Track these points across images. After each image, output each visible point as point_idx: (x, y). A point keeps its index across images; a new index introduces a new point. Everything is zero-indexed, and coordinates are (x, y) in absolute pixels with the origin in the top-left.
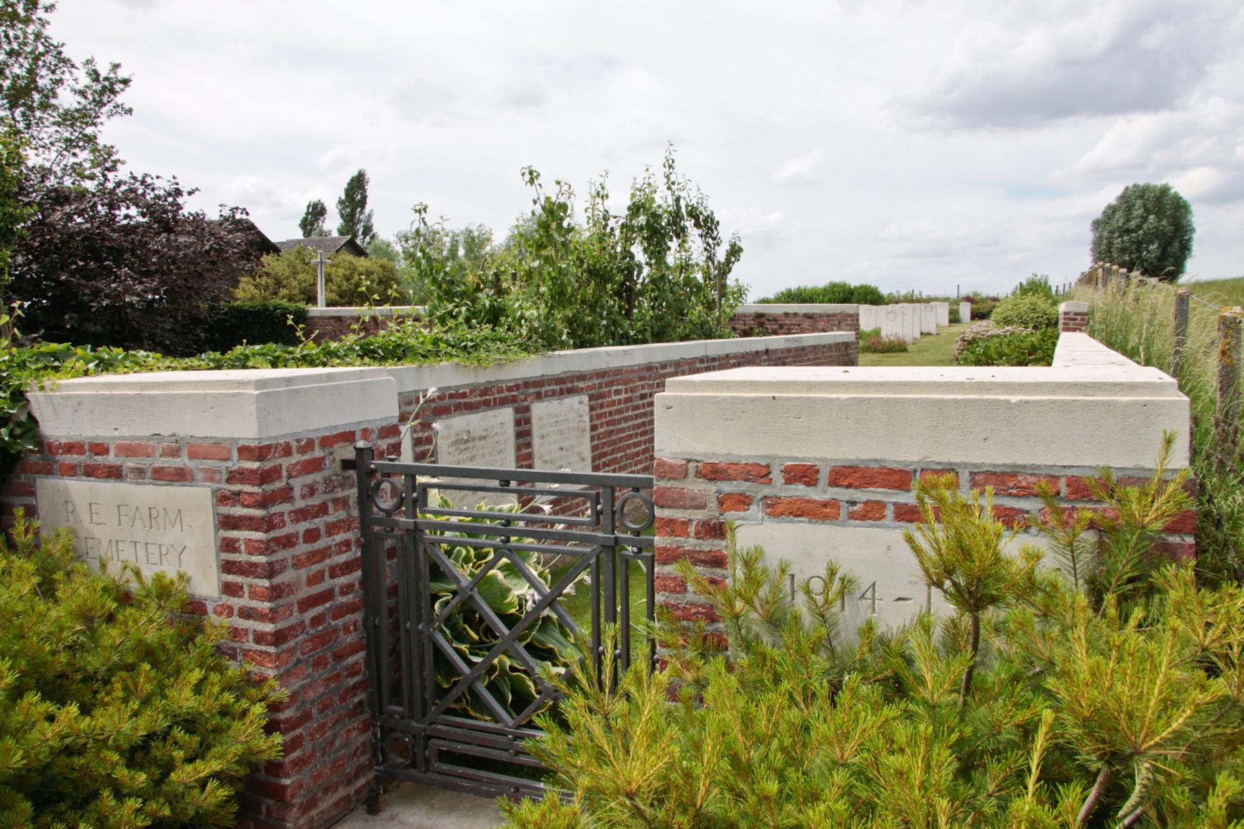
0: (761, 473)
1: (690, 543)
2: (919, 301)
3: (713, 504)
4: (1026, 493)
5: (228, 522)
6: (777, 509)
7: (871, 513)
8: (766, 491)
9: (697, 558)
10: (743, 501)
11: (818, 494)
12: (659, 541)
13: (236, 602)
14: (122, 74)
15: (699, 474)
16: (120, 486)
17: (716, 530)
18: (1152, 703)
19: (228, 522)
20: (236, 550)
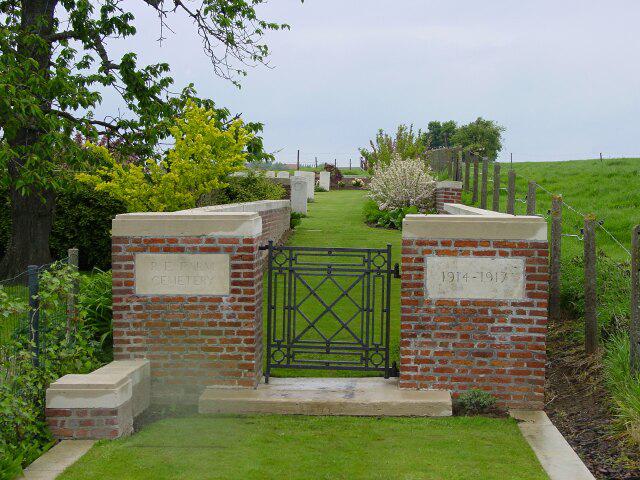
0: (435, 244)
1: (413, 264)
2: (239, 416)
3: (420, 253)
4: (505, 246)
5: (235, 267)
6: (439, 253)
7: (466, 254)
8: (436, 248)
9: (414, 269)
10: (430, 252)
11: (452, 248)
12: (543, 369)
13: (237, 296)
14: (130, 23)
15: (417, 244)
16: (183, 255)
17: (421, 260)
18: (82, 177)
19: (235, 267)
20: (239, 276)
